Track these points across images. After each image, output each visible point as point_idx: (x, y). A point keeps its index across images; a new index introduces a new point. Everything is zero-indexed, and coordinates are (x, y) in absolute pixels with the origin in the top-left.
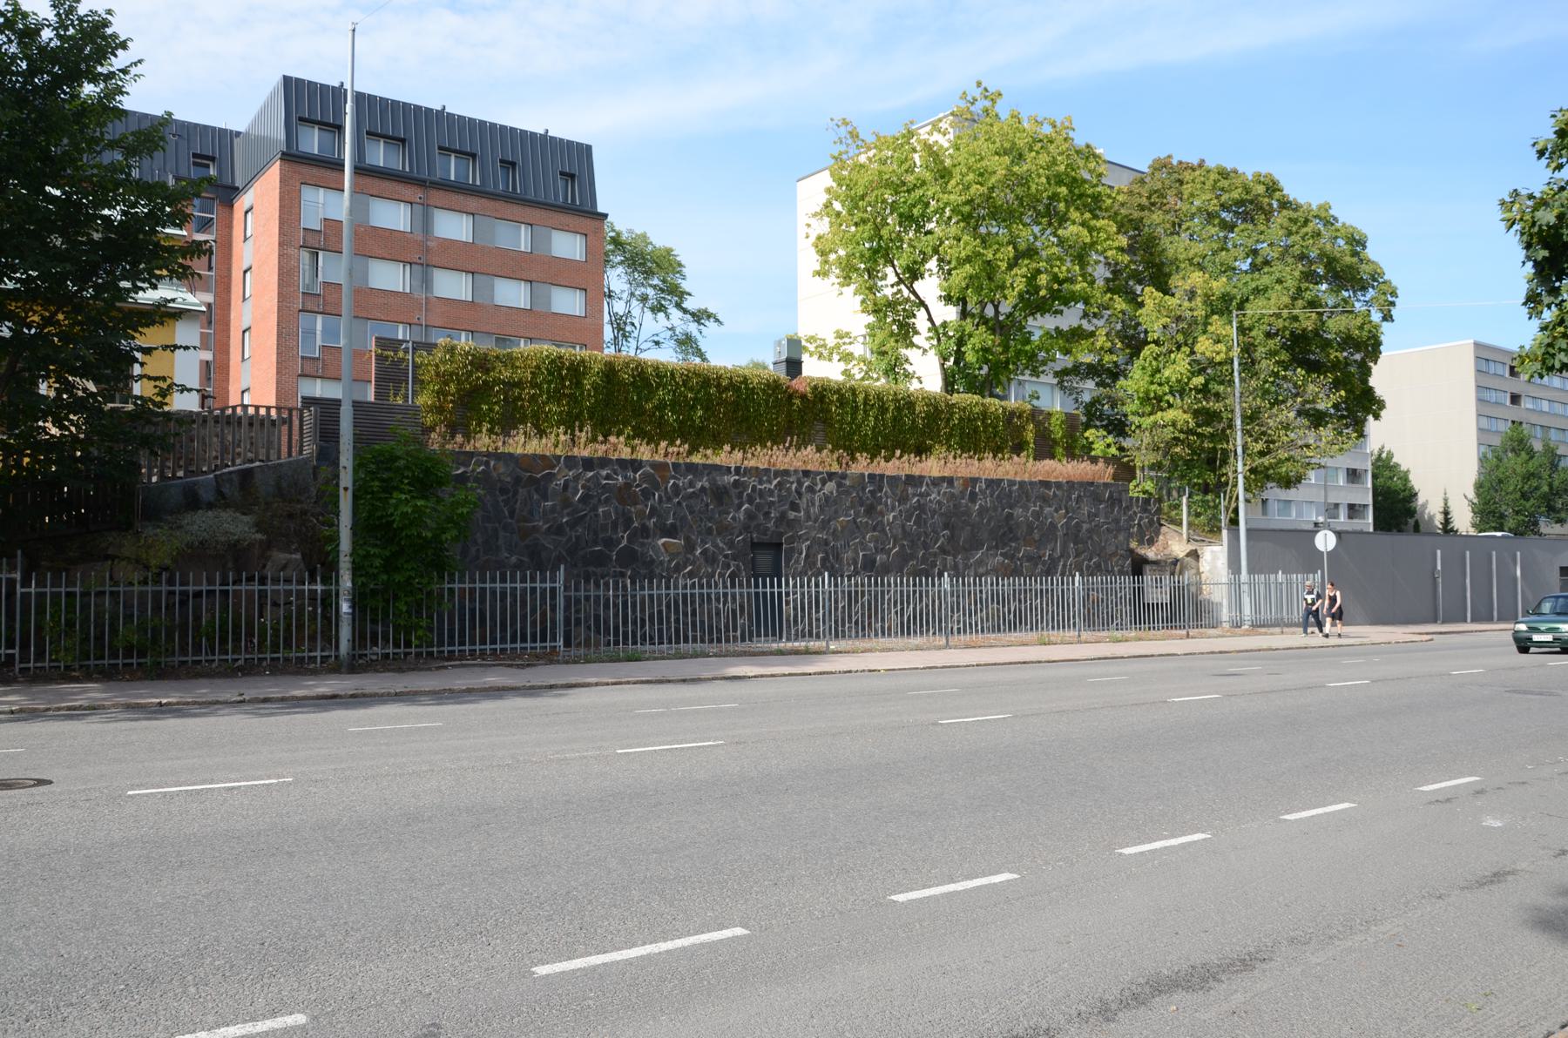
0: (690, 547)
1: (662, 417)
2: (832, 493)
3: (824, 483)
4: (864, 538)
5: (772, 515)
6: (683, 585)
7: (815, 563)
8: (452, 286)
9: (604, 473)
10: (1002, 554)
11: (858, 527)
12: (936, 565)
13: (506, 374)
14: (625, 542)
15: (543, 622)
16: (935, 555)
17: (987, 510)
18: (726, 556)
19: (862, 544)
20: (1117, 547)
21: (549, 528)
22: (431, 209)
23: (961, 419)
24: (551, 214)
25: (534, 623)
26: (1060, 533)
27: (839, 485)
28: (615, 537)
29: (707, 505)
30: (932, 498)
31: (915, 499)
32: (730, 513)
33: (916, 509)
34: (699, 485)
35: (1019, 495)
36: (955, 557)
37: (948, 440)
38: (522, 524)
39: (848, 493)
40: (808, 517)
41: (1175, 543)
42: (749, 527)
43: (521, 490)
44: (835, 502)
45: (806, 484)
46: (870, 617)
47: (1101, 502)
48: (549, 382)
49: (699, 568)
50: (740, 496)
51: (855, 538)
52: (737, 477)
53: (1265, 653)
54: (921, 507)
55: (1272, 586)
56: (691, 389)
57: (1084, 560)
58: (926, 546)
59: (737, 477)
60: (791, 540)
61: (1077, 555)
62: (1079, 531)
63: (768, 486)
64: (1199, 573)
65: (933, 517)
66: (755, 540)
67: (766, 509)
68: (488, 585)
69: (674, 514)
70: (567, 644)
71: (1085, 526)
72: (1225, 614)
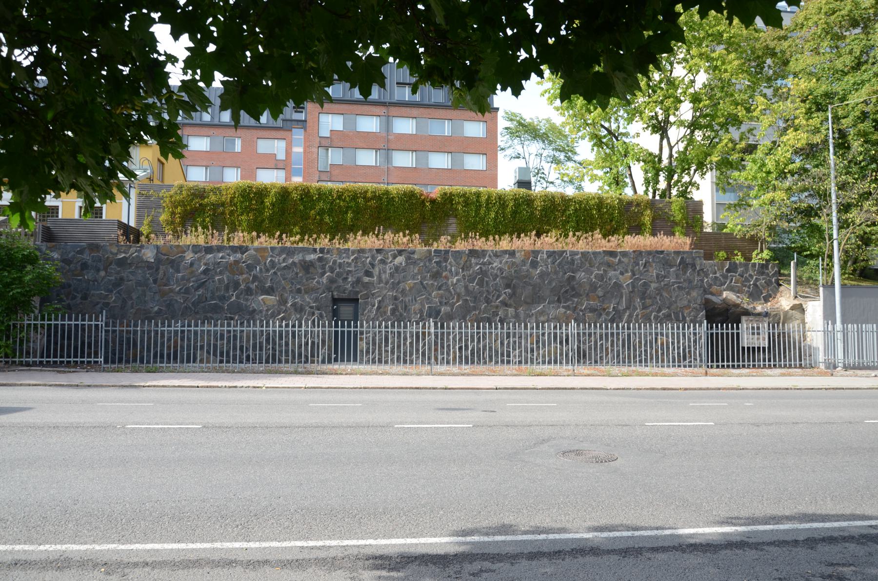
0: (283, 302)
1: (322, 220)
2: (401, 264)
3: (395, 257)
4: (430, 294)
5: (350, 280)
6: (275, 326)
7: (385, 313)
8: (403, 160)
9: (221, 255)
10: (563, 307)
11: (424, 287)
12: (497, 315)
13: (213, 198)
14: (234, 298)
15: (176, 347)
16: (497, 307)
17: (548, 274)
18: (311, 307)
19: (428, 299)
20: (689, 301)
21: (180, 289)
22: (391, 118)
23: (576, 210)
24: (355, 107)
25: (169, 348)
26: (625, 291)
27: (408, 258)
28: (227, 295)
29: (297, 274)
30: (494, 265)
31: (478, 267)
32: (315, 278)
33: (478, 274)
34: (291, 261)
35: (582, 262)
36: (516, 309)
37: (564, 226)
38: (162, 287)
39: (415, 263)
40: (380, 280)
41: (785, 301)
42: (331, 287)
43: (161, 267)
44: (404, 270)
45: (379, 258)
46: (436, 350)
47: (671, 266)
48: (242, 202)
49: (290, 315)
50: (323, 267)
51: (422, 295)
52: (321, 255)
53: (735, 391)
54: (483, 273)
55: (849, 334)
56: (344, 201)
57: (652, 312)
58: (488, 301)
59: (321, 255)
60: (366, 297)
61: (645, 307)
62: (647, 289)
63: (346, 260)
64: (803, 322)
65: (495, 280)
66: (336, 297)
67: (345, 276)
68: (225, 329)
69: (271, 280)
70: (106, 362)
71: (653, 285)
72: (821, 357)
